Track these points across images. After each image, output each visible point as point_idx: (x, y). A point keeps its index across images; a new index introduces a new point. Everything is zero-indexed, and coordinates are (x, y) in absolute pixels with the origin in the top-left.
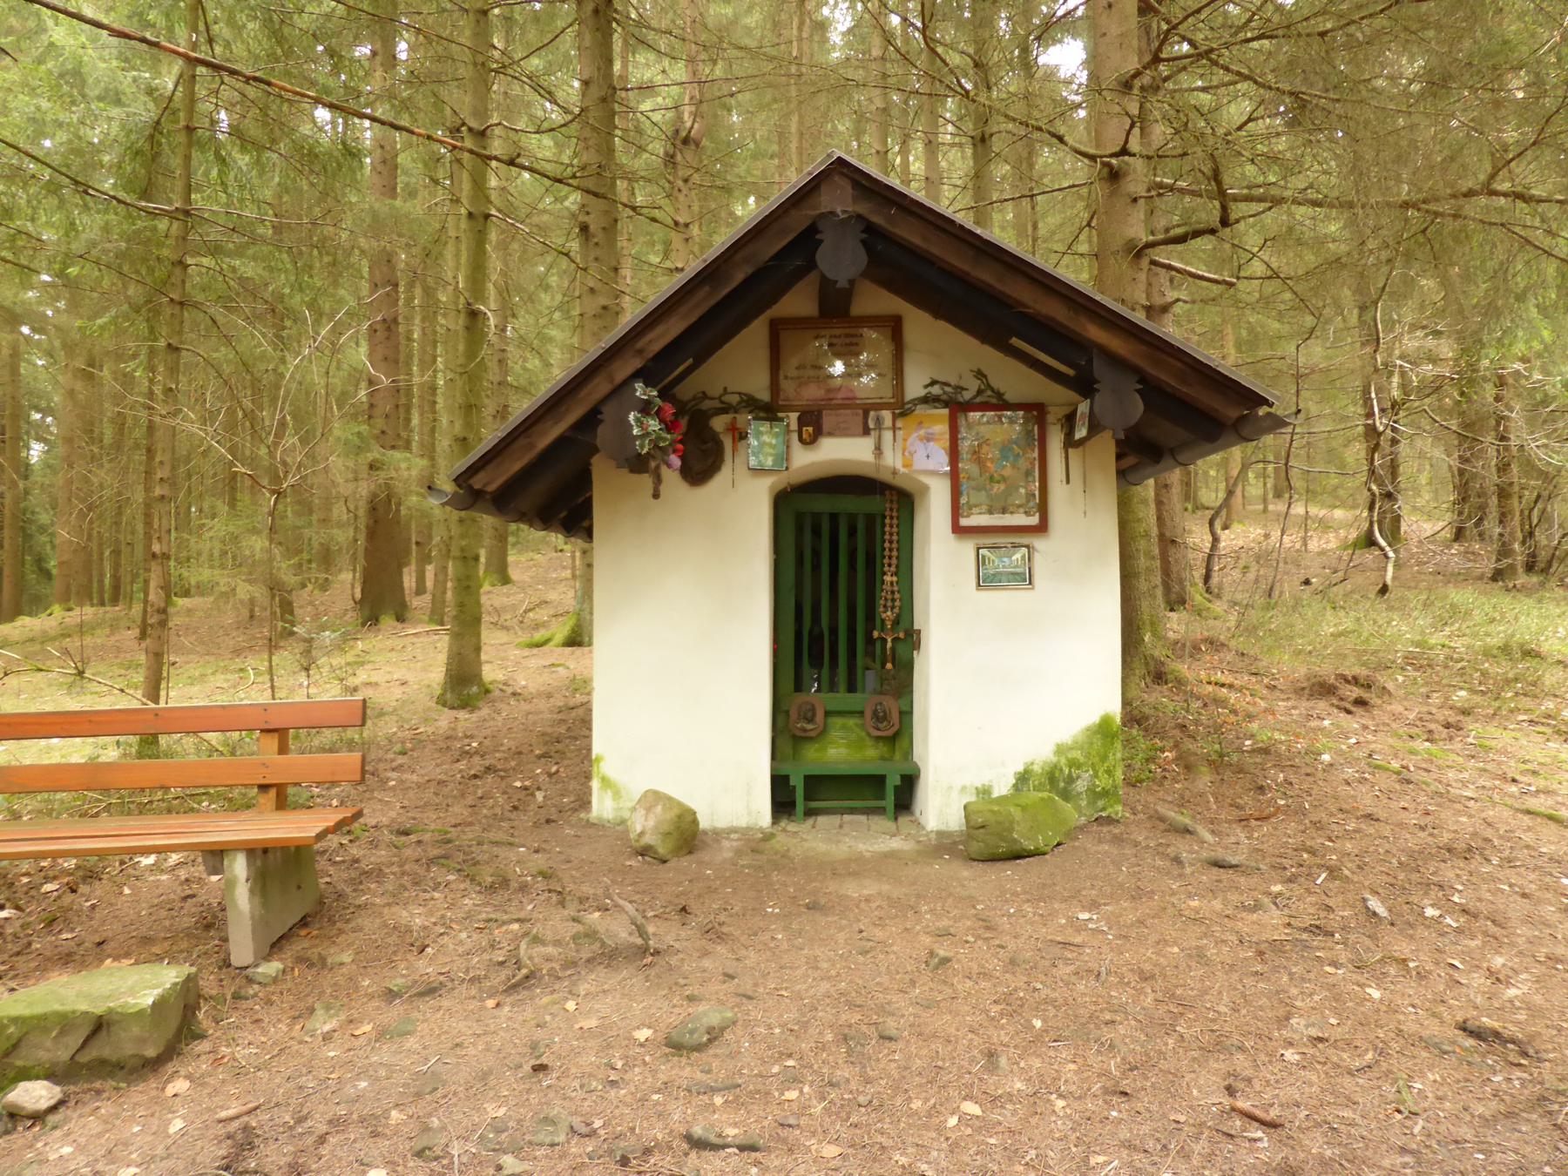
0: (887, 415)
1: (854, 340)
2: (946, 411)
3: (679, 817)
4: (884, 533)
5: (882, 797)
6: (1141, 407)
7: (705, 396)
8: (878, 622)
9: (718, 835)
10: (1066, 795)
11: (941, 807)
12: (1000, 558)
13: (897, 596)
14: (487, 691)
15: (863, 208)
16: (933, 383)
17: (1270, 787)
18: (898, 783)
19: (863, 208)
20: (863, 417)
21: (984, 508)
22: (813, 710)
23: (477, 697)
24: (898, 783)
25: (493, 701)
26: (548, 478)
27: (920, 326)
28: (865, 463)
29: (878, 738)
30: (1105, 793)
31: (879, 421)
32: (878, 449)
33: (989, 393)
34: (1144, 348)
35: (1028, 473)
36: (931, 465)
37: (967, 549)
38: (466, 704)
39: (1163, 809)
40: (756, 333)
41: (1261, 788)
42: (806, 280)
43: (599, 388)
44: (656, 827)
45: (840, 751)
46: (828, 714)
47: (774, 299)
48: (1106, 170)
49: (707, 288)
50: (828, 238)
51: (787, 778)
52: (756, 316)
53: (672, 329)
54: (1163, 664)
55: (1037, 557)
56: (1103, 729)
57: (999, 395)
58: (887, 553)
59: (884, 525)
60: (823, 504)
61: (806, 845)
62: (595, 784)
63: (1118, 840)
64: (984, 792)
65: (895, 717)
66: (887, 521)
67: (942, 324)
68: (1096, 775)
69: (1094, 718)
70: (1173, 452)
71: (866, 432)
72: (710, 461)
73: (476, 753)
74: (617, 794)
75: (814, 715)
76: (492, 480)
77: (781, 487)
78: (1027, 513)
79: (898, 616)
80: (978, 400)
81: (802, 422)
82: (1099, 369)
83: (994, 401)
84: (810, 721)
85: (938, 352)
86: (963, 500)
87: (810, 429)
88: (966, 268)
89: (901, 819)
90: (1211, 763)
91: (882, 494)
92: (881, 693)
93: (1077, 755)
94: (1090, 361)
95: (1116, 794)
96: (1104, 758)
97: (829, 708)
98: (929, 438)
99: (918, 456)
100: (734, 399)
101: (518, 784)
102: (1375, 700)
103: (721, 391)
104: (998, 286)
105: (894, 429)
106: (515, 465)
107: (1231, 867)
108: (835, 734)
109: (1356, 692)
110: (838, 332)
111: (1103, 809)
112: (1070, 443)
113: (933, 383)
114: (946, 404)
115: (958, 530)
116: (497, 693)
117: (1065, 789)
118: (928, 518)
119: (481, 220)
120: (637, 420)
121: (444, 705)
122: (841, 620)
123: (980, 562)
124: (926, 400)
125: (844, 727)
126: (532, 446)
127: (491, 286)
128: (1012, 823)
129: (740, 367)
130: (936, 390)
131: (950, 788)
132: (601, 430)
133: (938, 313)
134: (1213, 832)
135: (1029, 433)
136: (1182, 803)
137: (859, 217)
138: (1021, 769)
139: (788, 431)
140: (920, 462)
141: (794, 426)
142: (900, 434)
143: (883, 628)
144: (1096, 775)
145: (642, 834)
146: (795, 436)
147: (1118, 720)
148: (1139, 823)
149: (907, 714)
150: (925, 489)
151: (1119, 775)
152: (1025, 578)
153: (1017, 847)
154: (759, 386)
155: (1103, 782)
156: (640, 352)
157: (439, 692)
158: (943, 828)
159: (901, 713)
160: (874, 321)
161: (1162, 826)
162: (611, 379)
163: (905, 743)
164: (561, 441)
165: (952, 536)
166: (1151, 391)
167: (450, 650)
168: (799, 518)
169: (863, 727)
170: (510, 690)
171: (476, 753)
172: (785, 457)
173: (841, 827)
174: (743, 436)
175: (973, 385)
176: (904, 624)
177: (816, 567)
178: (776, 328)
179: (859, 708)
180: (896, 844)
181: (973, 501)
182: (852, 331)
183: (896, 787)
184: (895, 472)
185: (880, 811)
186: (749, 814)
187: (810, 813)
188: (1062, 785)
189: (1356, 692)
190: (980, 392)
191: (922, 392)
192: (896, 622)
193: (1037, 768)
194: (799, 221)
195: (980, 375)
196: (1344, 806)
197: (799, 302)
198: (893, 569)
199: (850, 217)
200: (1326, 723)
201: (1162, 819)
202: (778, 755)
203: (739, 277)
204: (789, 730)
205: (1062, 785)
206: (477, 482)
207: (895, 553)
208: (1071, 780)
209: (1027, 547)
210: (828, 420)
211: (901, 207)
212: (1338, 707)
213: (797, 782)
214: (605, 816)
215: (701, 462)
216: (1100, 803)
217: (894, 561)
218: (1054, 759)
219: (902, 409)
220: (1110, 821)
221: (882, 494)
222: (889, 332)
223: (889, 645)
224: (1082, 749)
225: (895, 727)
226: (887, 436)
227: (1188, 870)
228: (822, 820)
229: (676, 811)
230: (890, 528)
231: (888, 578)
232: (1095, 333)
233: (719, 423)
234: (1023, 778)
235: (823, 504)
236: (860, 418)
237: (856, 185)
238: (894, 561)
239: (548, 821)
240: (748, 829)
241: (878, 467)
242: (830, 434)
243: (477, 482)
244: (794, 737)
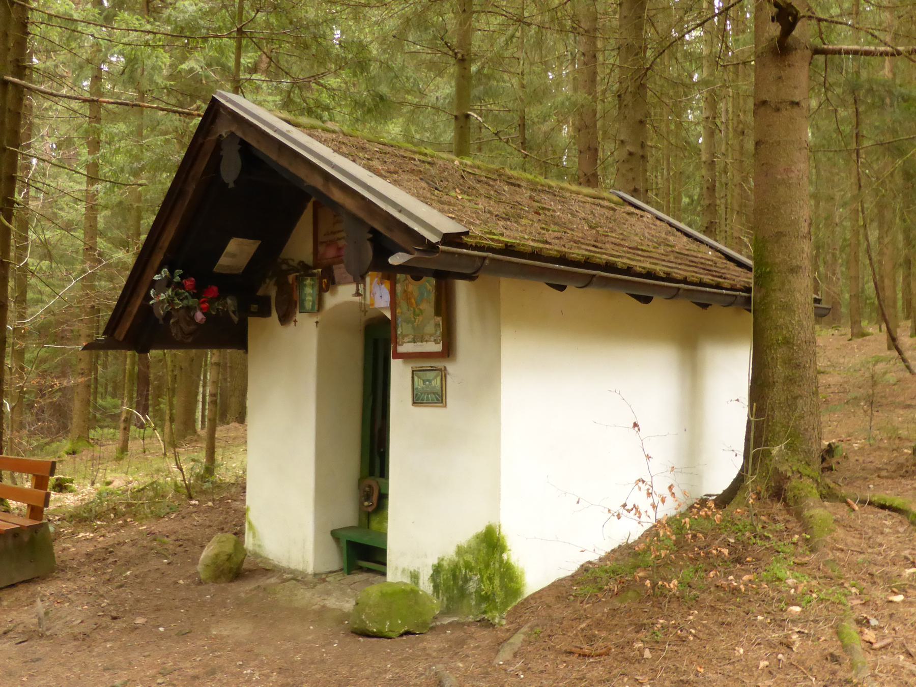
93: (469, 558)
111: (485, 612)
117: (462, 586)
127: (9, 288)
138: (436, 562)
152: (439, 399)
165: (704, 311)
181: (404, 333)
193: (445, 563)
208: (466, 580)
214: (57, 548)
216: (484, 606)
218: (456, 559)
242: (340, 284)
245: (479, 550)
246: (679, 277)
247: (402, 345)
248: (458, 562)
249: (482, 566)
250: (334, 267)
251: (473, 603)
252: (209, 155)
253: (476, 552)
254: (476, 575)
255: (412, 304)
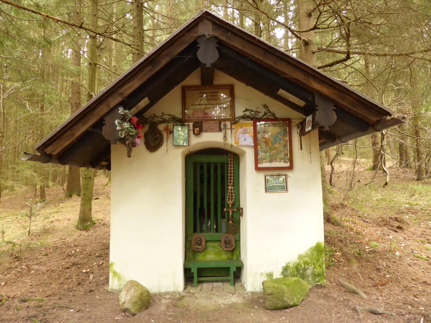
0: (228, 123)
1: (215, 94)
2: (252, 122)
3: (141, 294)
4: (228, 170)
5: (228, 275)
6: (335, 117)
7: (155, 116)
8: (226, 206)
9: (161, 296)
10: (303, 276)
11: (253, 280)
12: (274, 180)
13: (233, 194)
14: (94, 223)
15: (217, 34)
16: (247, 110)
17: (382, 269)
18: (235, 270)
19: (217, 34)
20: (219, 125)
21: (268, 160)
22: (201, 240)
23: (90, 226)
24: (235, 270)
25: (96, 227)
26: (84, 148)
27: (241, 88)
28: (221, 143)
29: (227, 251)
30: (319, 275)
31: (225, 126)
32: (225, 137)
33: (269, 114)
34: (336, 92)
35: (285, 146)
36: (246, 143)
37: (261, 176)
38: (86, 229)
39: (342, 281)
40: (176, 92)
41: (378, 269)
42: (196, 71)
43: (103, 110)
44: (130, 300)
45: (212, 256)
46: (207, 241)
47: (183, 79)
48: (304, 42)
49: (150, 67)
50: (202, 46)
51: (190, 269)
52: (176, 85)
53: (135, 84)
54: (329, 215)
55: (289, 180)
56: (318, 249)
57: (273, 115)
58: (229, 178)
59: (228, 167)
60: (205, 159)
61: (197, 301)
62: (111, 275)
63: (326, 297)
64: (270, 275)
65: (233, 243)
66: (229, 165)
67: (250, 88)
68: (315, 268)
69: (313, 244)
70: (340, 138)
71: (220, 130)
72: (157, 142)
73: (73, 255)
74: (120, 279)
75: (201, 242)
76: (55, 149)
77: (187, 152)
78: (285, 162)
79: (234, 202)
80: (265, 117)
81: (194, 127)
82: (318, 101)
83: (271, 117)
84: (200, 245)
85: (248, 98)
86: (259, 157)
87: (198, 129)
88: (261, 58)
89: (236, 285)
90: (356, 258)
91: (227, 155)
92: (228, 233)
93: (307, 259)
94: (313, 98)
95: (323, 275)
96: (318, 260)
97: (207, 239)
98: (245, 132)
99: (240, 139)
100: (167, 117)
101: (84, 271)
102: (404, 227)
103: (161, 114)
104: (275, 66)
105: (231, 129)
106: (66, 143)
107: (380, 314)
108: (209, 249)
109: (397, 224)
110: (208, 91)
111: (319, 281)
112: (302, 133)
113: (247, 110)
114: (252, 119)
115: (258, 169)
116: (97, 224)
117: (303, 274)
118: (245, 164)
119: (94, 65)
120: (119, 123)
121: (78, 229)
122: (211, 203)
123: (266, 181)
124: (244, 117)
125: (213, 247)
126: (73, 135)
128: (283, 292)
129: (170, 104)
130: (248, 113)
131: (256, 274)
132: (104, 128)
133: (248, 84)
134: (365, 292)
135: (285, 130)
136: (349, 277)
137: (215, 37)
139: (189, 130)
140: (242, 142)
141: (191, 128)
142: (234, 131)
143: (228, 207)
144: (315, 268)
145: (124, 303)
146: (192, 132)
147: (323, 244)
148: (333, 288)
149: (238, 241)
150: (244, 153)
151: (324, 266)
152: (284, 188)
153: (286, 304)
154: (177, 112)
155: (318, 270)
156: (121, 94)
157: (77, 224)
158: (254, 290)
159: (236, 241)
160: (222, 87)
161: (343, 290)
162: (108, 105)
163: (237, 252)
164: (87, 134)
165: (255, 171)
166: (340, 110)
167: (81, 210)
168: (195, 164)
169: (221, 246)
170: (103, 223)
171: (73, 255)
172: (189, 141)
173: (212, 290)
174: (172, 132)
175: (263, 111)
176: (236, 205)
177: (202, 182)
178: (184, 90)
179: (219, 239)
180: (234, 299)
182: (215, 91)
183: (234, 272)
184: (232, 146)
185: (229, 281)
186: (174, 286)
187: (199, 282)
188: (301, 272)
189: (397, 224)
190: (265, 114)
191: (242, 114)
192: (233, 205)
193: (291, 265)
194: (189, 39)
195: (265, 106)
196: (414, 278)
197: (193, 79)
198: (232, 184)
199: (212, 37)
200: (391, 237)
201: (342, 286)
202: (187, 258)
203: (164, 62)
204: (191, 248)
205: (301, 272)
206: (48, 150)
207: (232, 178)
208: (305, 270)
209: (285, 175)
210: (205, 126)
211: (233, 33)
212: (392, 230)
213: (194, 271)
214: (115, 288)
215: (154, 143)
216: (317, 279)
217: (232, 181)
218: (298, 261)
219: (234, 121)
220: (321, 286)
221: (227, 155)
222: (228, 91)
223: (231, 214)
224: (309, 257)
225: (233, 246)
226: (229, 131)
227: (361, 316)
228: (205, 285)
229: (140, 292)
230: (230, 167)
231: (230, 188)
232: (316, 85)
233: (161, 127)
234: (286, 269)
235: (205, 159)
236: (218, 125)
237: (214, 23)
238: (232, 181)
239: (91, 291)
240: (174, 292)
241: (225, 144)
242: (206, 131)
243: (48, 150)
244: (194, 251)
245: (313, 255)
246: (68, 131)
247: (261, 163)
248: (300, 262)
249: (315, 261)
250: (203, 122)
251: (310, 279)
252: (186, 45)
253: (311, 256)
254: (311, 266)
255: (269, 144)
